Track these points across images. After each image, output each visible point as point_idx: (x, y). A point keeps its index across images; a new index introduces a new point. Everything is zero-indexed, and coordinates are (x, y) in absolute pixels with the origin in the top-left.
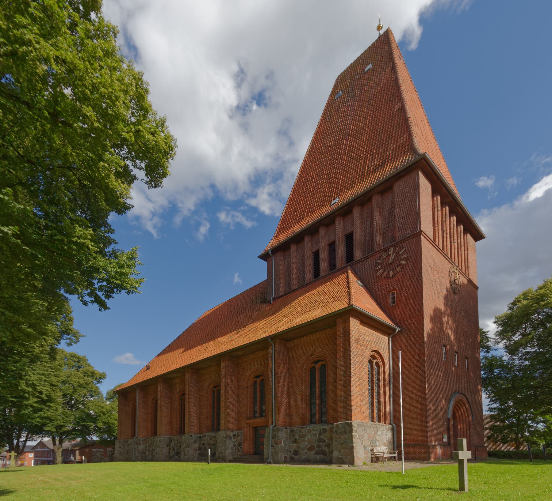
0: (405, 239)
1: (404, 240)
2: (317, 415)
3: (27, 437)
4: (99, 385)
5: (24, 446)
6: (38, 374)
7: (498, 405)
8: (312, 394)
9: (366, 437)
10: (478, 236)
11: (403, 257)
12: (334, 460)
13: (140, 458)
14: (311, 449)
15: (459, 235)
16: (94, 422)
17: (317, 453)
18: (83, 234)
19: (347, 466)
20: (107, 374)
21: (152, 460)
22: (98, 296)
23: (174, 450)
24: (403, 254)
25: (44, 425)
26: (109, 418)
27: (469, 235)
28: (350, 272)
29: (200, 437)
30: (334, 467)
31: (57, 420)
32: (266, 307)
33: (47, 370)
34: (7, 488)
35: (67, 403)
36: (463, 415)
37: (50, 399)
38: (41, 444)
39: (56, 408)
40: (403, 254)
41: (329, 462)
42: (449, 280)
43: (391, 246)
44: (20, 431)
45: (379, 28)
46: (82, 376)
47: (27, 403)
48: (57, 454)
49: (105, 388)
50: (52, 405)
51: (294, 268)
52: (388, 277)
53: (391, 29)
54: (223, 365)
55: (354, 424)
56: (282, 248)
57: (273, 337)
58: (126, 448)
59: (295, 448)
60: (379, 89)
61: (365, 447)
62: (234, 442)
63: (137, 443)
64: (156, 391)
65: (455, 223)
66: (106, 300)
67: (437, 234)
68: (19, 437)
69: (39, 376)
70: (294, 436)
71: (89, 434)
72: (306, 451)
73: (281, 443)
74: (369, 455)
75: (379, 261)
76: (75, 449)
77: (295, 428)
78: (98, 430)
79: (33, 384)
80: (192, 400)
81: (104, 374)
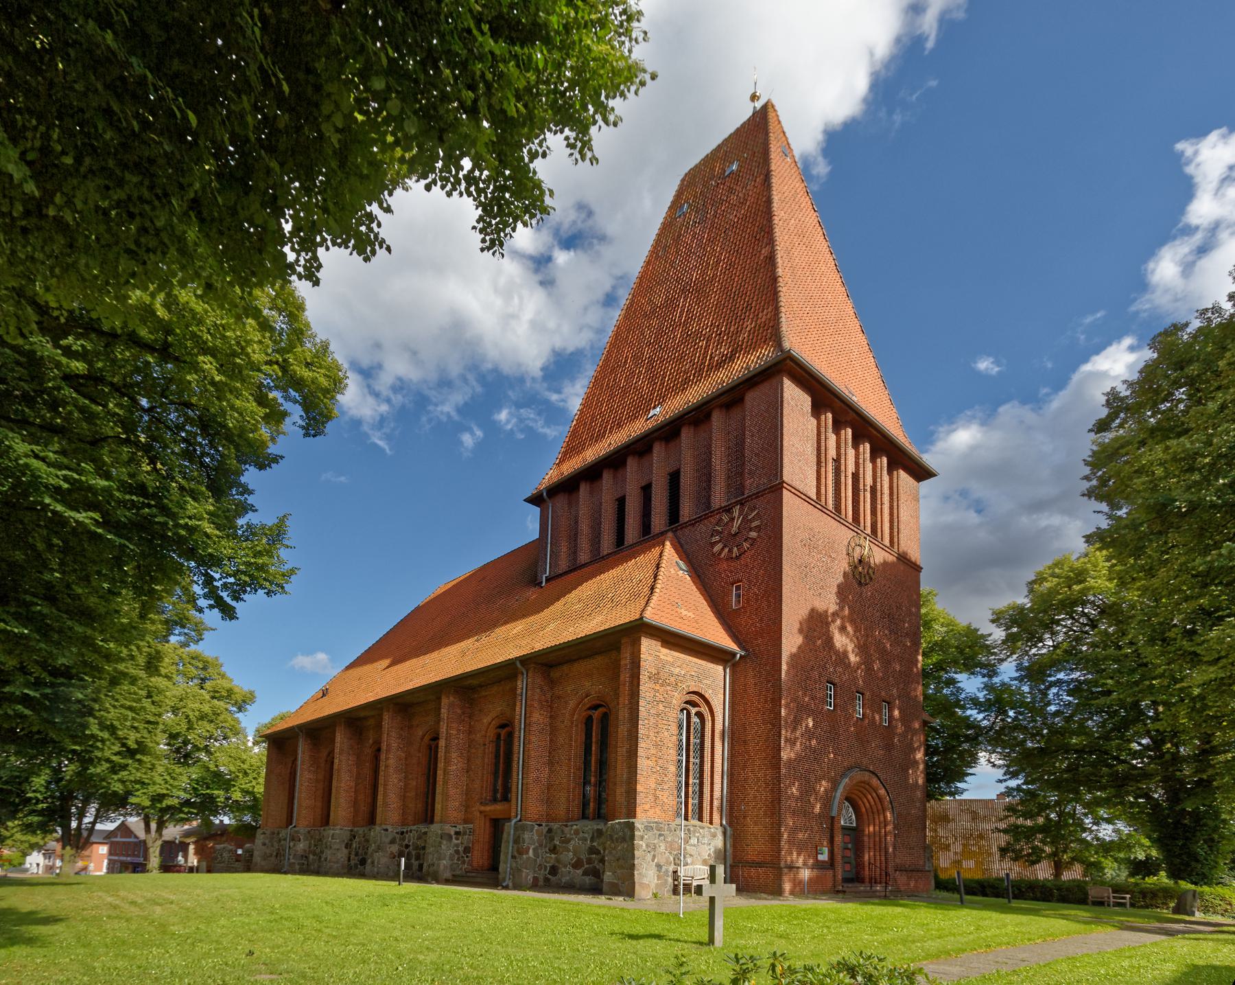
1: (757, 495)
2: (592, 804)
3: (97, 817)
4: (240, 715)
5: (91, 830)
6: (122, 706)
7: (1020, 782)
8: (587, 763)
9: (662, 847)
10: (921, 473)
12: (605, 888)
13: (297, 867)
14: (577, 865)
16: (227, 790)
17: (585, 873)
18: (198, 512)
19: (621, 898)
20: (256, 694)
21: (318, 872)
22: (221, 598)
23: (357, 855)
24: (753, 519)
25: (129, 793)
26: (254, 783)
27: (902, 473)
28: (668, 543)
29: (402, 833)
30: (602, 900)
31: (154, 783)
32: (532, 594)
33: (139, 701)
34: (55, 913)
35: (178, 751)
37: (142, 748)
38: (124, 829)
39: (153, 765)
40: (753, 519)
41: (596, 890)
43: (736, 503)
44: (86, 802)
45: (754, 97)
46: (208, 697)
47: (99, 754)
48: (151, 850)
49: (253, 721)
50: (144, 758)
51: (584, 527)
52: (730, 558)
53: (774, 102)
54: (445, 701)
55: (637, 825)
56: (566, 488)
57: (525, 660)
58: (276, 845)
59: (552, 862)
61: (659, 866)
62: (457, 845)
63: (293, 839)
64: (333, 741)
65: (868, 455)
66: (233, 603)
67: (823, 480)
68: (81, 815)
69: (123, 711)
70: (552, 839)
71: (216, 813)
72: (569, 868)
73: (527, 853)
74: (670, 880)
76: (188, 840)
77: (555, 826)
78: (236, 807)
79: (112, 725)
80: (392, 762)
81: (252, 693)
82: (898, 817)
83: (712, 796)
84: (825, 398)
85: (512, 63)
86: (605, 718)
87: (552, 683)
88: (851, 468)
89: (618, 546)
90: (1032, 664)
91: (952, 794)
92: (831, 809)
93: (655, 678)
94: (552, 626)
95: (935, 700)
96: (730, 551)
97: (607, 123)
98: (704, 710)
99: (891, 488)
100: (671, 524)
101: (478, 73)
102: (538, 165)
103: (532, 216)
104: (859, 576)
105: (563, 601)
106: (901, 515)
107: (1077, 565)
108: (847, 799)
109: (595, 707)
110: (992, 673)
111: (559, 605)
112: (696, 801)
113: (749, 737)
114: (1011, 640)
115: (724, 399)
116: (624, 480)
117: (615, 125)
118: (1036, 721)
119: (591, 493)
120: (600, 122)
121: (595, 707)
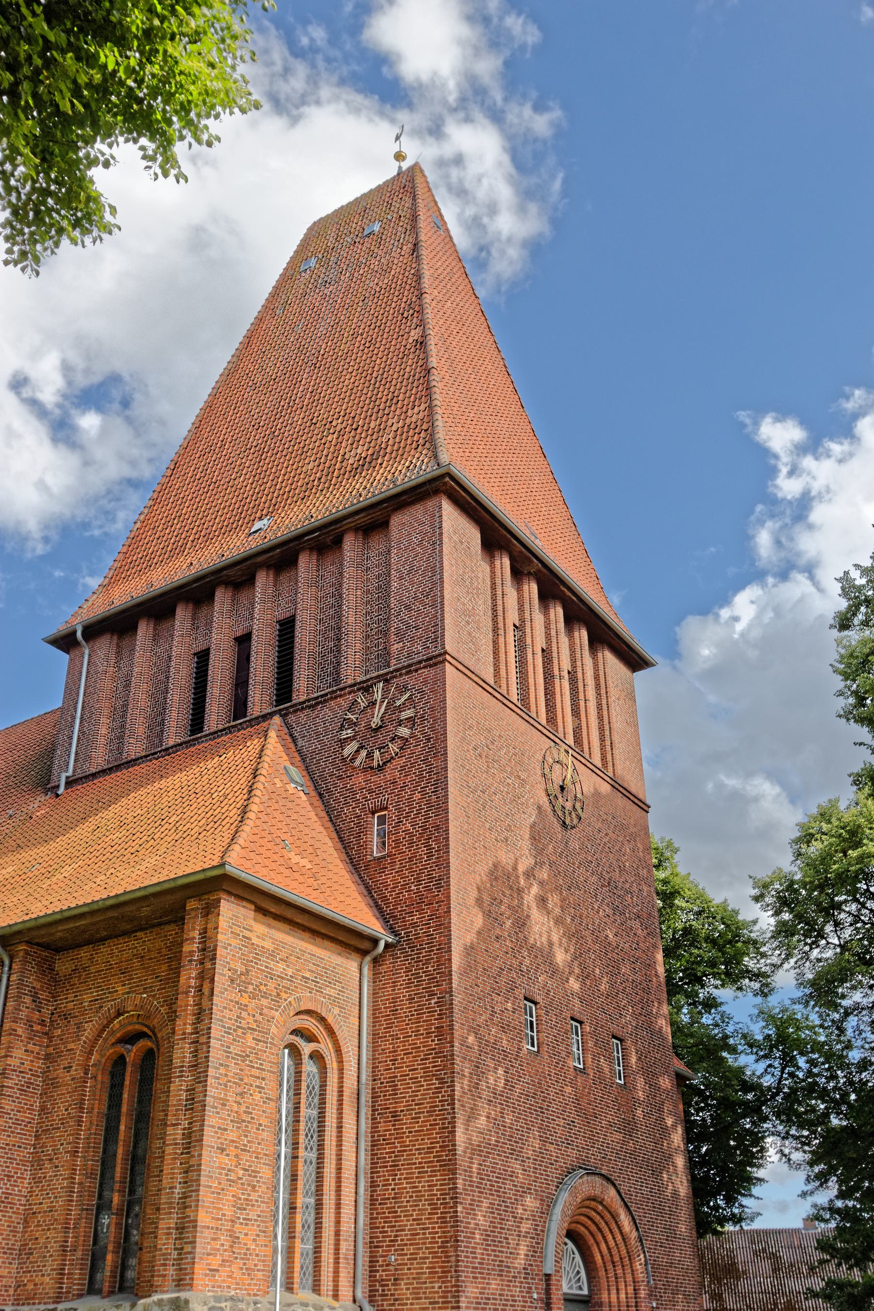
0: (410, 666)
1: (409, 669)
2: (109, 1257)
11: (405, 715)
15: (578, 656)
28: (272, 734)
32: (38, 805)
36: (614, 1251)
42: (543, 786)
52: (368, 768)
60: (386, 281)
75: (350, 716)
82: (652, 1266)
83: (337, 1233)
84: (496, 536)
85: (70, 55)
86: (150, 1056)
87: (55, 983)
88: (540, 642)
89: (193, 732)
90: (819, 976)
91: (737, 1220)
92: (542, 1258)
93: (239, 980)
94: (67, 871)
95: (691, 1035)
96: (370, 755)
97: (199, 142)
98: (326, 1047)
99: (597, 678)
100: (279, 702)
101: (22, 56)
102: (96, 173)
103: (86, 232)
104: (565, 810)
105: (93, 821)
106: (613, 720)
107: (847, 818)
108: (571, 1235)
109: (131, 1039)
110: (765, 992)
111: (84, 830)
112: (310, 1247)
113: (401, 1107)
114: (784, 931)
115: (361, 519)
116: (209, 624)
117: (209, 144)
118: (836, 1077)
119: (156, 638)
120: (189, 138)
121: (131, 1039)
